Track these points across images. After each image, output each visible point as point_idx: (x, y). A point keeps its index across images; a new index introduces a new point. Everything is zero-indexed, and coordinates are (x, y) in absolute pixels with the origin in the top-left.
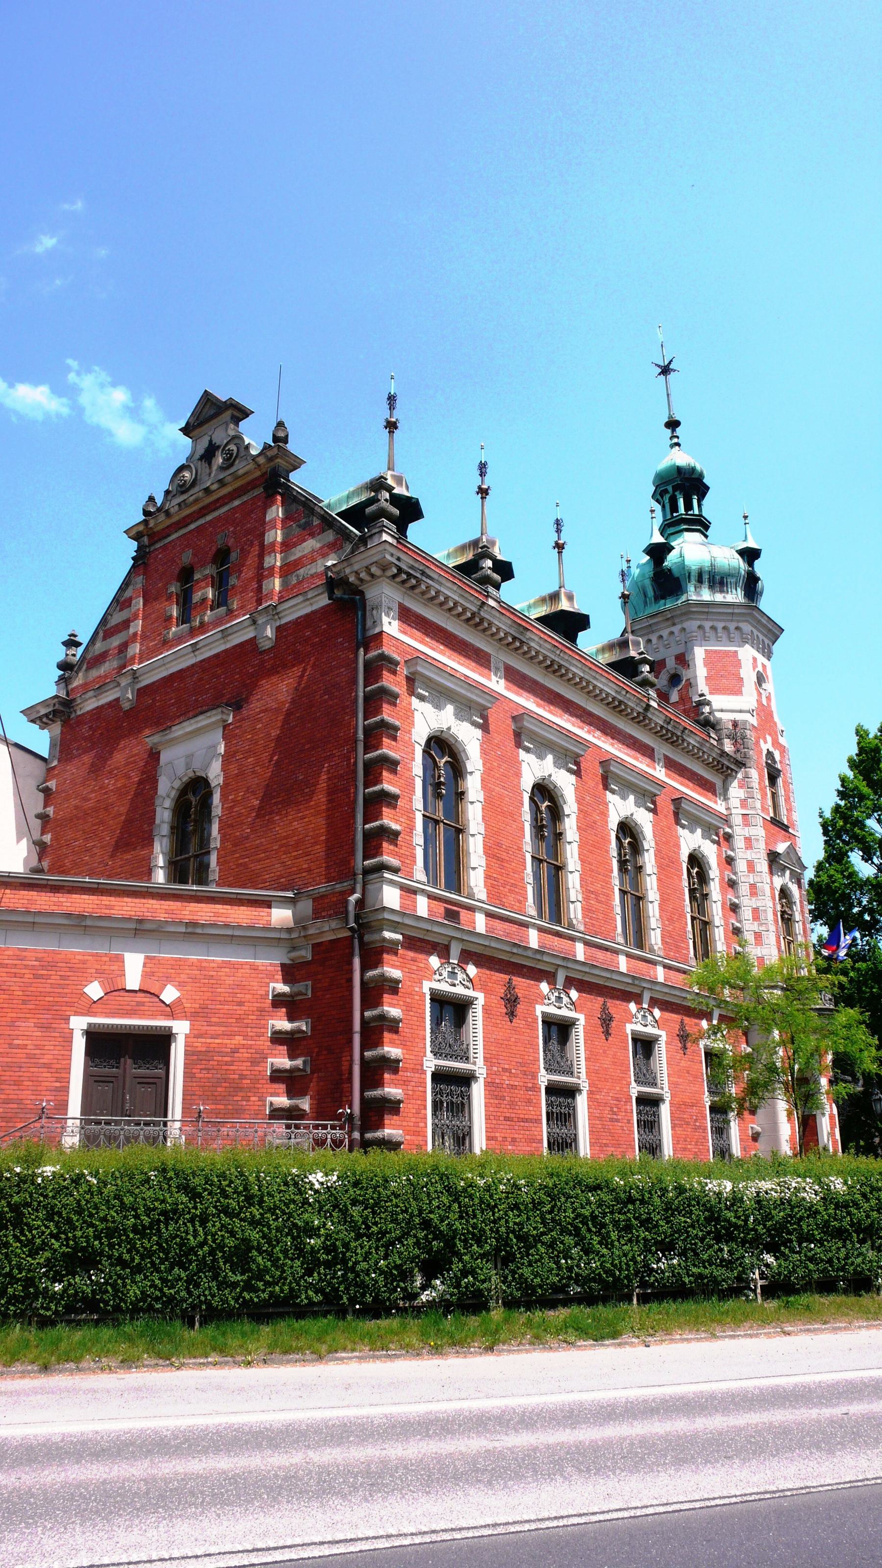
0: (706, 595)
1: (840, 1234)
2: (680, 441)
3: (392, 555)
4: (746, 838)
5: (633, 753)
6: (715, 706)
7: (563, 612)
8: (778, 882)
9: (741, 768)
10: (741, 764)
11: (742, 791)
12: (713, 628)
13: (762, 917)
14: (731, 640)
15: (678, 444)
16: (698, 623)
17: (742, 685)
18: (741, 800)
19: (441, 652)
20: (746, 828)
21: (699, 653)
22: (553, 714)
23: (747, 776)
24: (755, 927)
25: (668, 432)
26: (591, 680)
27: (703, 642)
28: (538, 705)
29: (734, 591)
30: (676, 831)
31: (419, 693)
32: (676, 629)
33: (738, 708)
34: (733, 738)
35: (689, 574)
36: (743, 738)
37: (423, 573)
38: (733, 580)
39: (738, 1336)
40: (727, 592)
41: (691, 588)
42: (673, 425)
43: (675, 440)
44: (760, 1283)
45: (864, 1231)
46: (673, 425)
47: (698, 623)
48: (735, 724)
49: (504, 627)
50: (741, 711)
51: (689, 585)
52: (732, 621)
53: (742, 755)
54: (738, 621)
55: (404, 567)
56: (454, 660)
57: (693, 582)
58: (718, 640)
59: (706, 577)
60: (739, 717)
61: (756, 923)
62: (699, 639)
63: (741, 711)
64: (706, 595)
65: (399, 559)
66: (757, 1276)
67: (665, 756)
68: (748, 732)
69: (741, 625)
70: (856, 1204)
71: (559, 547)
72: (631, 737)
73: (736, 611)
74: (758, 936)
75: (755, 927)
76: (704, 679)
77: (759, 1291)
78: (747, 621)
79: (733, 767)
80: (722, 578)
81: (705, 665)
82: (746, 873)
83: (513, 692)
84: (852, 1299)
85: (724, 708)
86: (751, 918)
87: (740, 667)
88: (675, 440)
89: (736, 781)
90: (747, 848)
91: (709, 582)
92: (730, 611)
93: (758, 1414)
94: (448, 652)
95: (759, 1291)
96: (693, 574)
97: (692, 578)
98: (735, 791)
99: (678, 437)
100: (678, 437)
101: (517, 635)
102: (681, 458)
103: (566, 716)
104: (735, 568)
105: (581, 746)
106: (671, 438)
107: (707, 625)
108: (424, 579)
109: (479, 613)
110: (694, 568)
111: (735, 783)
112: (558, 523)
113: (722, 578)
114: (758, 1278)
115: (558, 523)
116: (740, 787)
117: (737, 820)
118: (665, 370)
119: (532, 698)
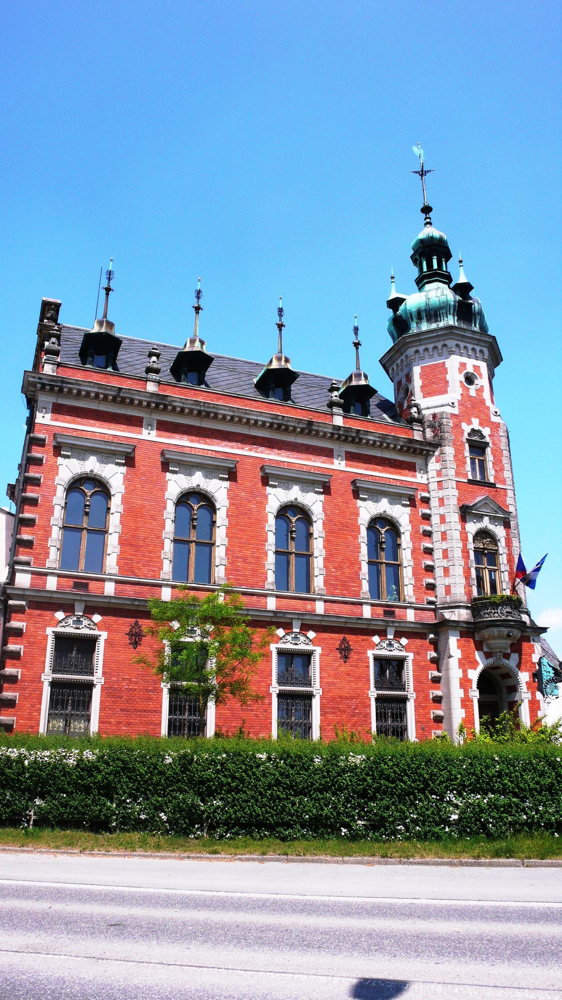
0: (425, 326)
1: (87, 790)
2: (432, 221)
3: (34, 377)
4: (440, 499)
5: (304, 456)
6: (422, 406)
7: (288, 369)
8: (472, 527)
9: (438, 448)
10: (438, 445)
11: (438, 464)
12: (465, 347)
13: (450, 556)
14: (440, 355)
15: (430, 223)
16: (415, 349)
17: (448, 386)
18: (437, 471)
19: (93, 425)
20: (440, 491)
21: (417, 371)
22: (209, 444)
23: (442, 453)
24: (445, 563)
25: (424, 216)
26: (243, 415)
27: (420, 362)
28: (192, 441)
29: (445, 319)
30: (355, 504)
31: (63, 454)
32: (403, 357)
33: (440, 404)
34: (432, 426)
35: (411, 315)
36: (441, 425)
37: (63, 382)
38: (444, 311)
39: (74, 853)
40: (441, 320)
41: (414, 325)
42: (427, 210)
43: (428, 220)
44: (33, 817)
45: (103, 788)
46: (427, 210)
47: (415, 349)
48: (434, 416)
49: (144, 399)
50: (442, 406)
51: (412, 323)
52: (439, 341)
53: (439, 438)
54: (444, 340)
55: (46, 382)
56: (103, 428)
57: (415, 320)
58: (431, 357)
59: (424, 314)
60: (437, 411)
61: (445, 560)
62: (417, 360)
63: (442, 406)
64: (425, 326)
65: (40, 378)
66: (32, 813)
67: (346, 452)
68: (444, 421)
69: (446, 342)
70: (97, 769)
71: (280, 326)
72: (303, 445)
73: (439, 333)
74: (446, 570)
75: (445, 563)
76: (420, 388)
77: (31, 823)
78: (451, 338)
79: (431, 449)
80: (436, 312)
81: (421, 378)
82: (439, 524)
83: (164, 437)
84: (92, 835)
85: (429, 406)
86: (441, 557)
87: (447, 373)
88: (428, 220)
89: (434, 458)
90: (440, 506)
91: (427, 317)
92: (435, 334)
93: (250, 915)
94: (98, 423)
95: (31, 823)
96: (413, 315)
97: (414, 318)
98: (433, 465)
99: (430, 218)
100: (430, 218)
101: (158, 401)
102: (433, 232)
103: (225, 443)
104: (444, 302)
105: (229, 461)
106: (425, 219)
107: (421, 348)
108: (65, 385)
109: (119, 395)
110: (413, 310)
111: (433, 459)
112: (281, 310)
113: (436, 312)
114: (32, 814)
115: (281, 310)
116: (437, 461)
117: (433, 486)
118: (422, 173)
119: (186, 437)
